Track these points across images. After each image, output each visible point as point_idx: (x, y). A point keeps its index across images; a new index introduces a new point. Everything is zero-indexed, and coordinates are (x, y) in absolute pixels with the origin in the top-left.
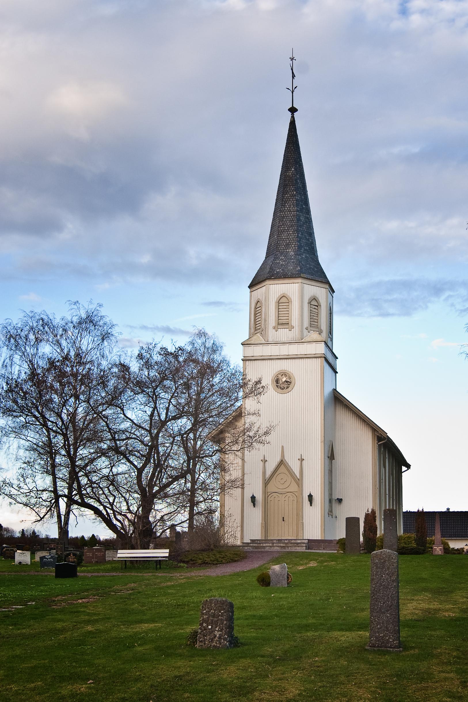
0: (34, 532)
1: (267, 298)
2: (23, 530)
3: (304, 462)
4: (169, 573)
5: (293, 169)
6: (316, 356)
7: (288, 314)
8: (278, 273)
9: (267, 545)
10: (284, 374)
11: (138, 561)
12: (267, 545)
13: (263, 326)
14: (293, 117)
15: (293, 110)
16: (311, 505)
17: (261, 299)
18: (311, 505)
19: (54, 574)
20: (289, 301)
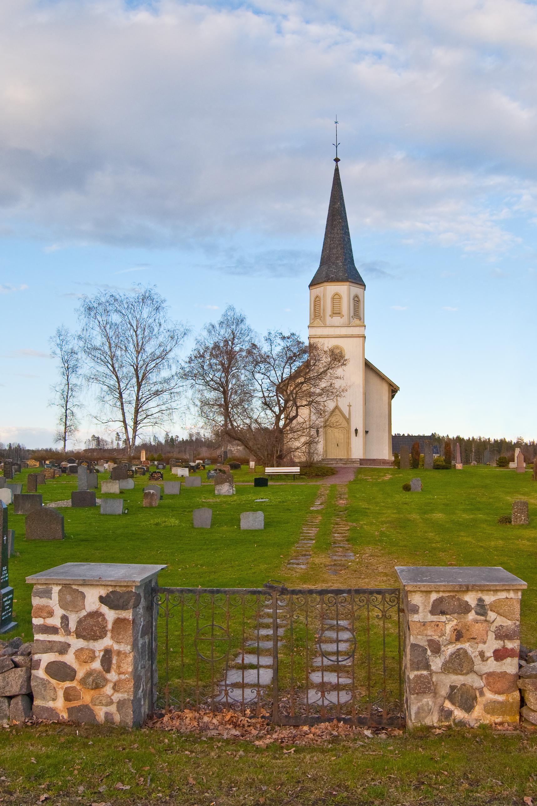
0: (19, 446)
1: (324, 295)
2: (10, 444)
3: (351, 407)
4: (316, 481)
5: (339, 204)
6: (359, 336)
7: (340, 308)
8: (332, 278)
9: (333, 462)
10: (337, 347)
11: (296, 476)
12: (333, 462)
13: (322, 314)
14: (337, 165)
15: (337, 160)
16: (356, 436)
17: (319, 295)
18: (356, 436)
19: (253, 484)
20: (340, 298)
